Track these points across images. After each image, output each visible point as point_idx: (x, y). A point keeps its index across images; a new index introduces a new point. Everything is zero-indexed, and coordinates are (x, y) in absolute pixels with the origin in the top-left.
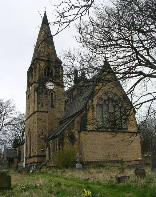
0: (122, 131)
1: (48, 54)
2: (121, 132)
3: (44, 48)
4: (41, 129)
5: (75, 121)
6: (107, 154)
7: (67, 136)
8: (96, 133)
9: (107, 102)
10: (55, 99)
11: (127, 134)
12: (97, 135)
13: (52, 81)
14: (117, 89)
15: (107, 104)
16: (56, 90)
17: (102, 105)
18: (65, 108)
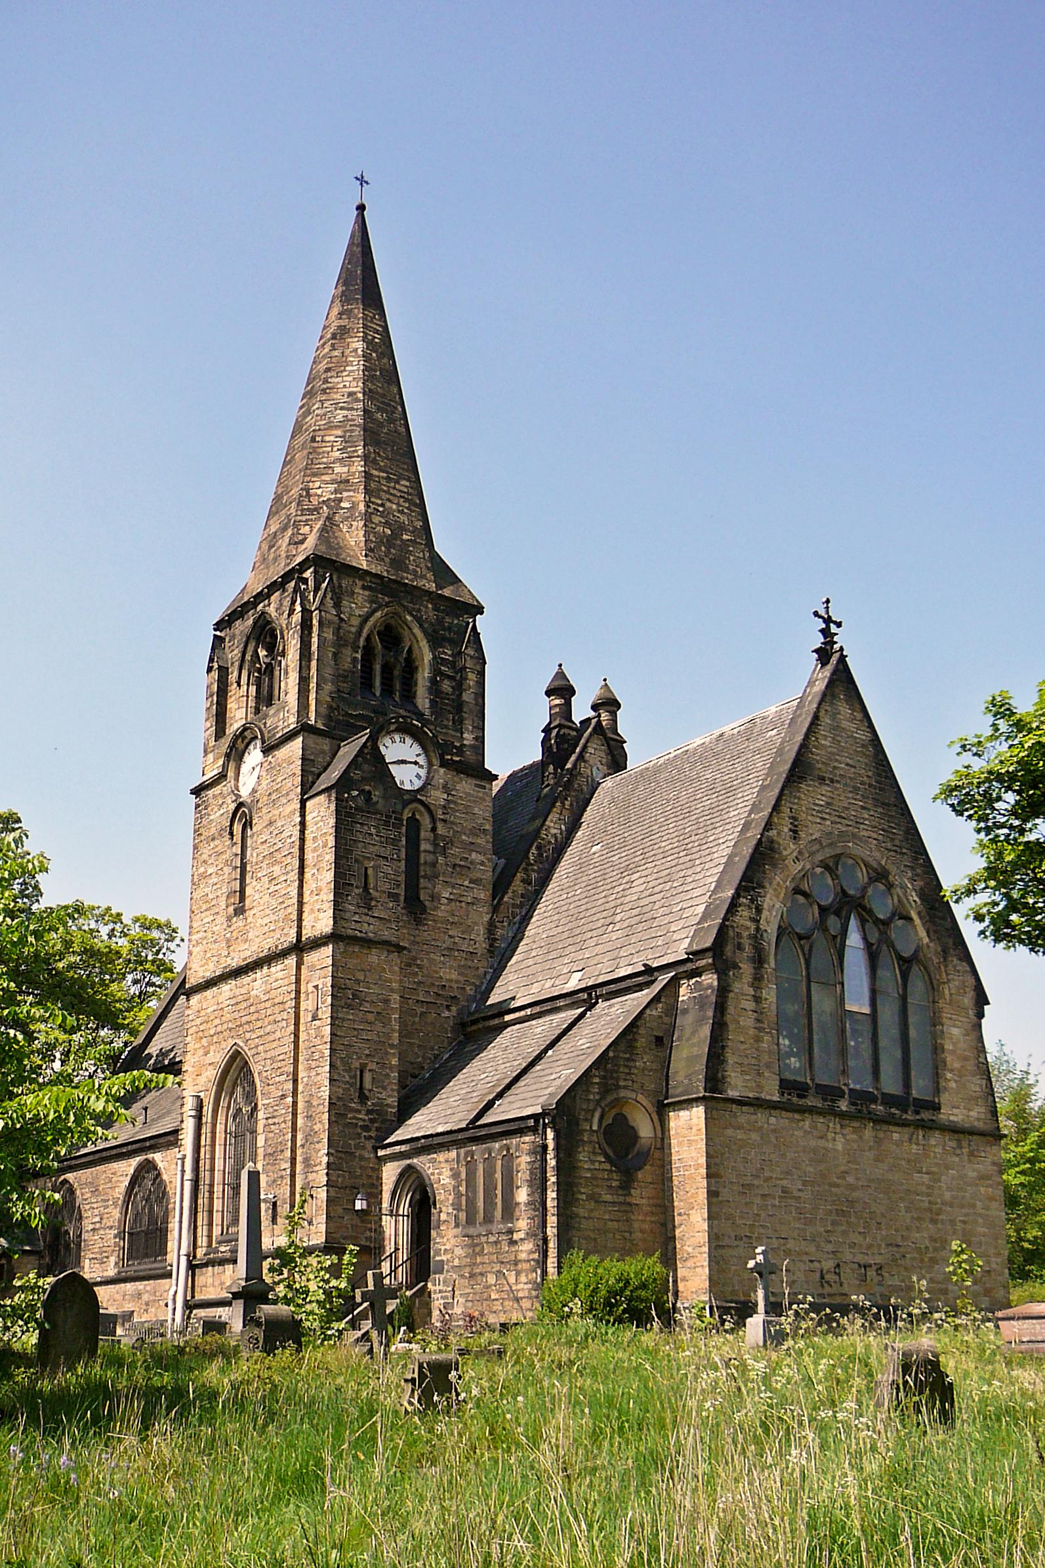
0: (910, 1116)
1: (396, 535)
2: (905, 1124)
3: (367, 491)
4: (356, 1064)
5: (642, 1031)
6: (829, 1265)
7: (595, 1128)
8: (773, 1120)
9: (833, 923)
10: (434, 864)
11: (935, 1139)
12: (774, 1131)
13: (417, 736)
14: (889, 845)
15: (834, 937)
16: (437, 797)
17: (807, 938)
18: (491, 927)
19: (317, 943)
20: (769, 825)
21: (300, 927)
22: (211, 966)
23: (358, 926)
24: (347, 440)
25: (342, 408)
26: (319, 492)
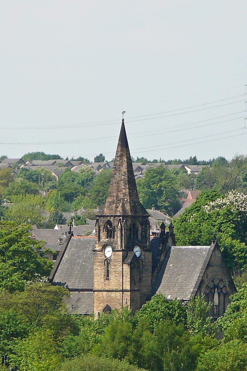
3: (129, 196)
15: (213, 293)
19: (127, 291)
20: (203, 277)
21: (123, 287)
22: (100, 287)
23: (133, 288)
24: (125, 184)
25: (123, 176)
26: (120, 196)
